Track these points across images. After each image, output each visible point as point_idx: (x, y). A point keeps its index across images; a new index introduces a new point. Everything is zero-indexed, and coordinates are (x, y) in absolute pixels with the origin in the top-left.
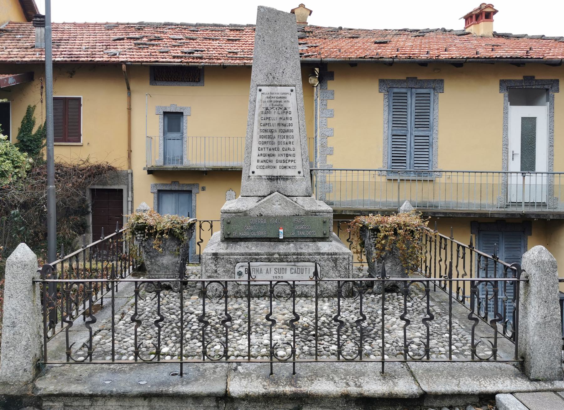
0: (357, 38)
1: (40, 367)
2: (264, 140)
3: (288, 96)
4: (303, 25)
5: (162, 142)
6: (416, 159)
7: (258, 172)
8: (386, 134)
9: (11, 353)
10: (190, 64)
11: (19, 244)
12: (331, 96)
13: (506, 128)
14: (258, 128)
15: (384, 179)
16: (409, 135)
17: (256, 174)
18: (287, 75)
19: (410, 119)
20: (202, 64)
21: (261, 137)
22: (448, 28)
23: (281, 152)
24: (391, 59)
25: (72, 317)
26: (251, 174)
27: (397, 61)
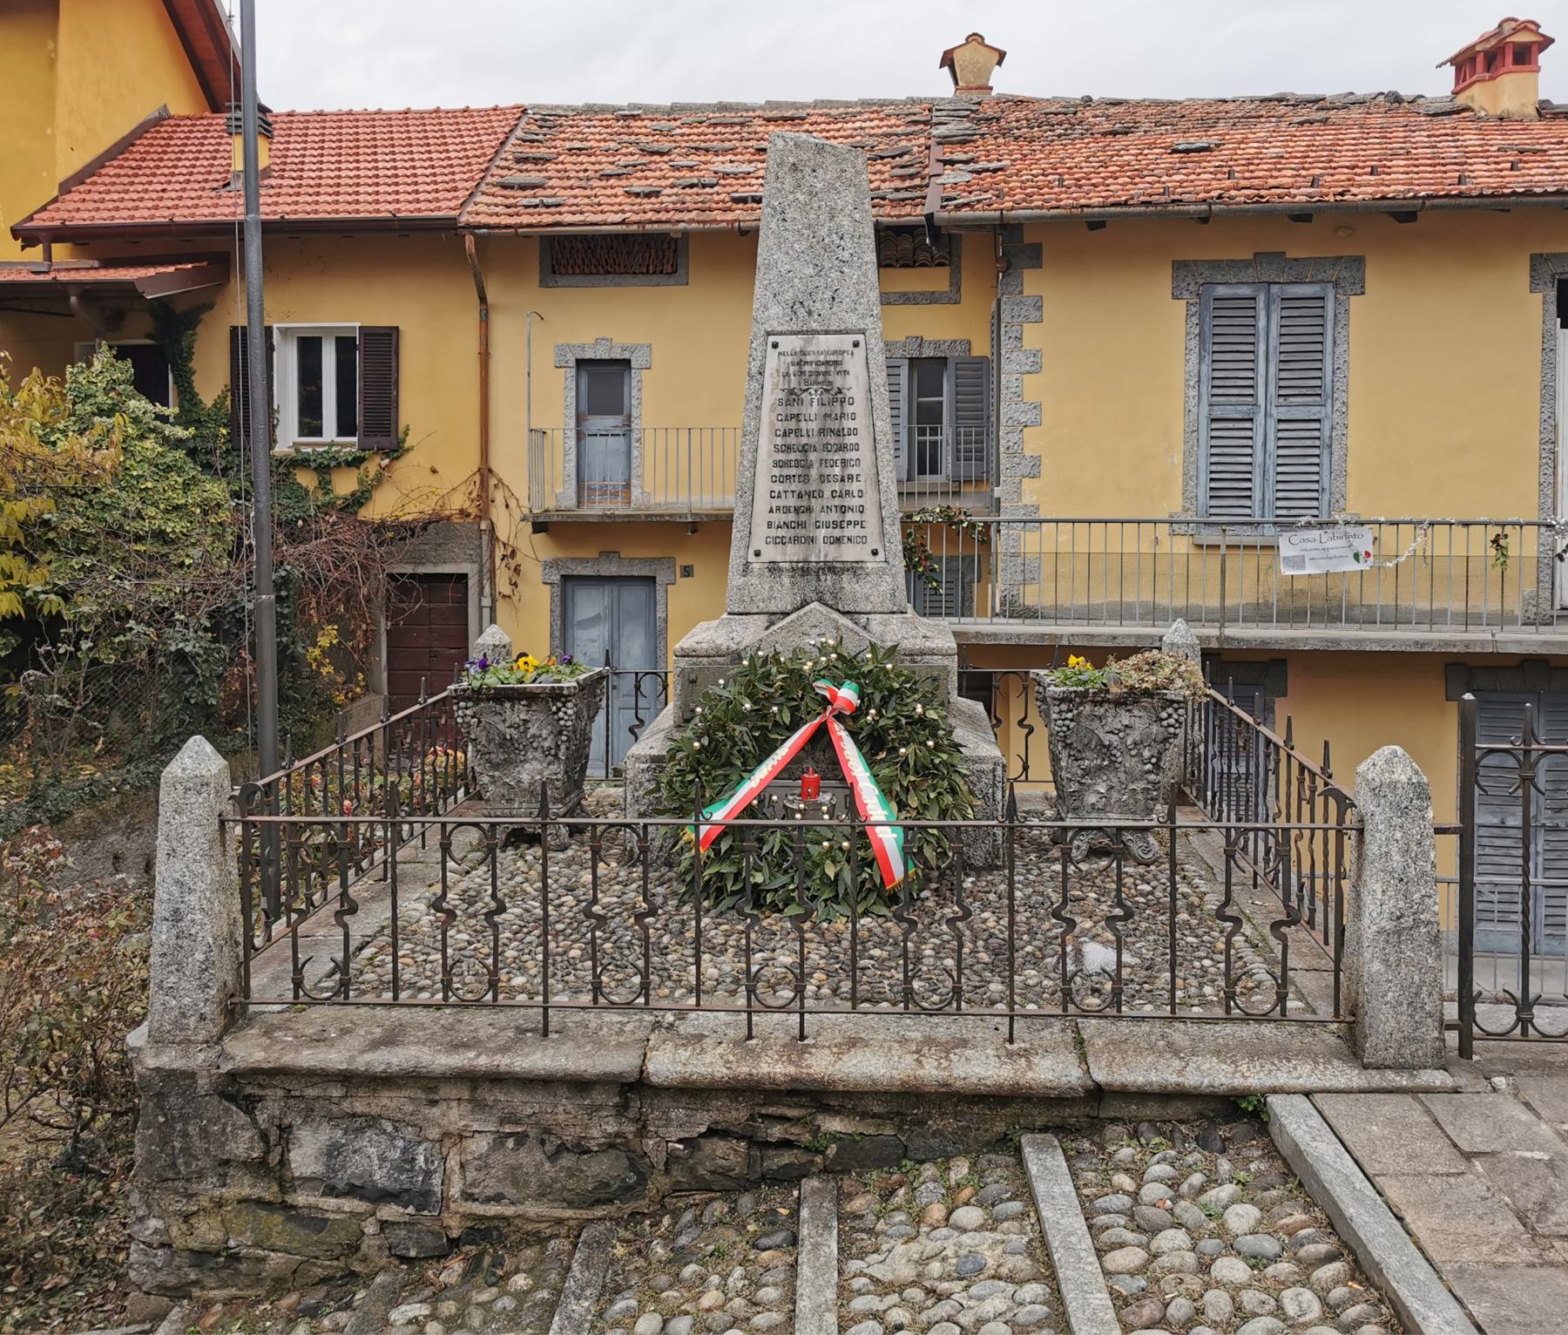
1: (235, 1011)
2: (786, 471)
4: (975, 96)
5: (573, 442)
6: (1280, 486)
7: (771, 553)
9: (172, 979)
10: (648, 227)
11: (193, 733)
12: (1034, 314)
14: (770, 441)
15: (1182, 546)
16: (1260, 419)
17: (765, 557)
18: (844, 306)
19: (1266, 371)
20: (682, 225)
21: (777, 464)
22: (1406, 92)
24: (1204, 207)
25: (310, 903)
26: (751, 558)
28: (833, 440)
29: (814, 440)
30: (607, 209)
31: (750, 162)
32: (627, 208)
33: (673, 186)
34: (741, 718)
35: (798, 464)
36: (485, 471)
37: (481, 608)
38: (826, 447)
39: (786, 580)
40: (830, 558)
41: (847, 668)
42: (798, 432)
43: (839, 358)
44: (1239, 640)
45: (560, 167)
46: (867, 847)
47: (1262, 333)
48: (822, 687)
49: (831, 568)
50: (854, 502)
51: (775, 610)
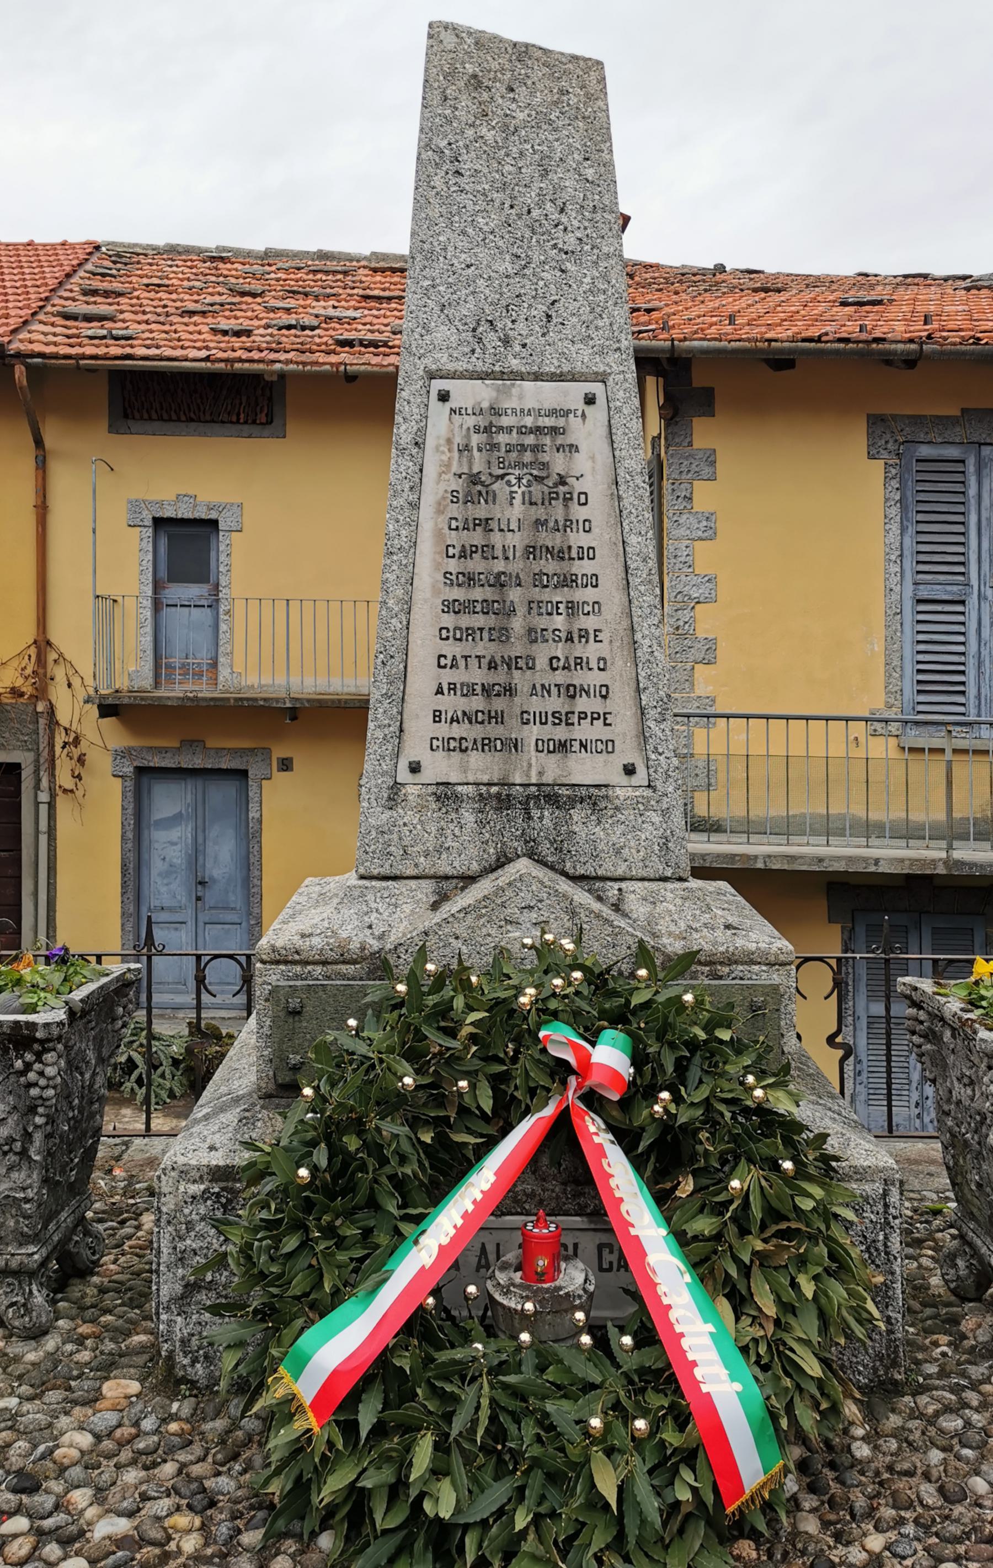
0: (779, 291)
2: (466, 621)
3: (574, 421)
5: (148, 614)
7: (439, 767)
8: (895, 597)
10: (238, 366)
12: (706, 471)
14: (437, 566)
16: (973, 601)
17: (428, 775)
23: (543, 676)
26: (403, 775)
27: (934, 352)
28: (551, 566)
29: (516, 566)
30: (191, 346)
31: (356, 309)
32: (212, 345)
33: (267, 327)
34: (393, 1103)
35: (487, 607)
36: (43, 644)
37: (37, 804)
38: (539, 580)
39: (468, 817)
40: (548, 778)
41: (604, 1001)
42: (487, 551)
43: (561, 422)
44: (972, 865)
45: (134, 301)
46: (682, 1419)
47: (973, 502)
48: (559, 1039)
49: (549, 796)
50: (593, 679)
51: (449, 871)
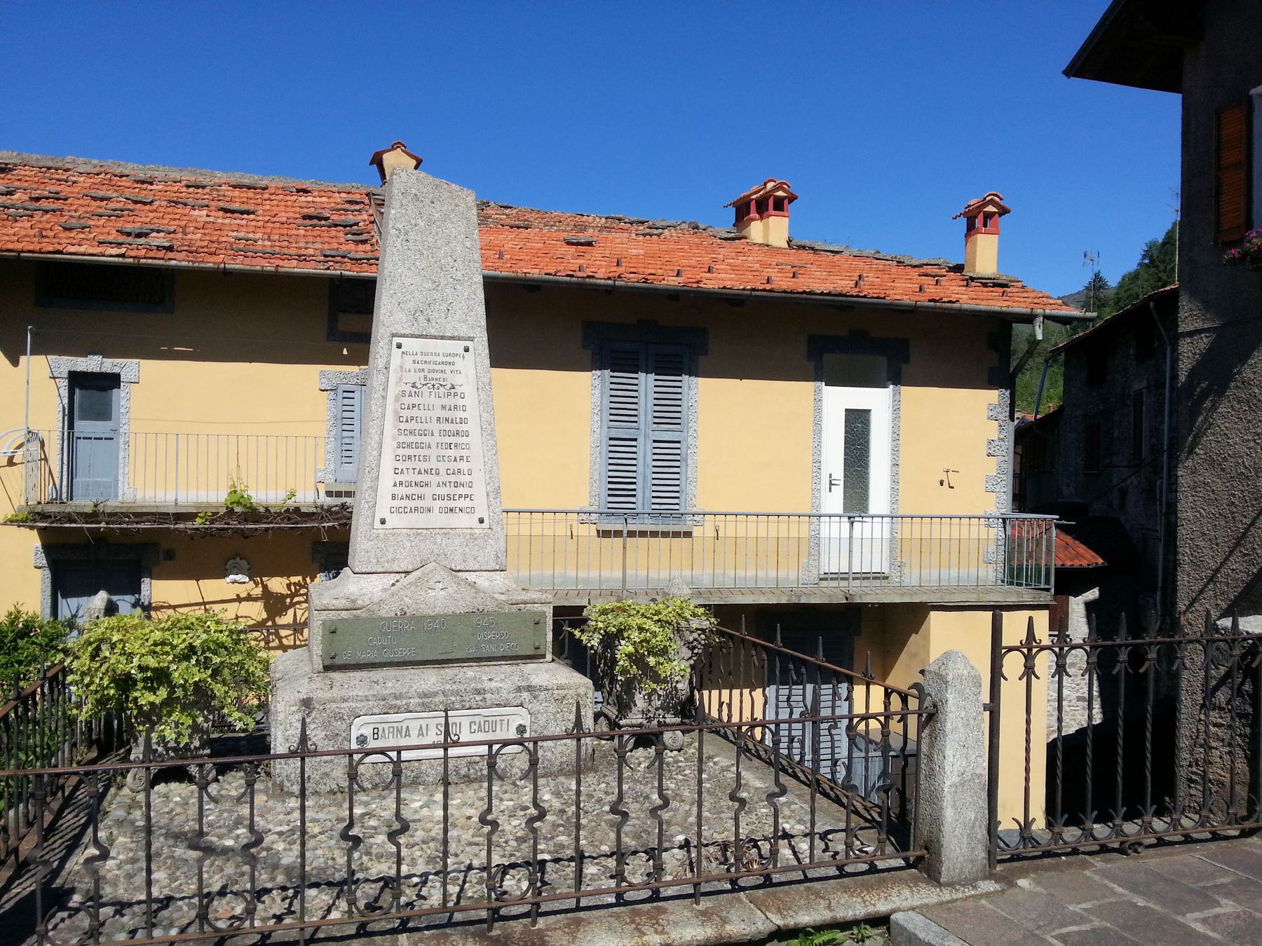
13: (818, 431)
14: (395, 427)
16: (641, 440)
17: (388, 525)
24: (610, 282)
27: (621, 287)
